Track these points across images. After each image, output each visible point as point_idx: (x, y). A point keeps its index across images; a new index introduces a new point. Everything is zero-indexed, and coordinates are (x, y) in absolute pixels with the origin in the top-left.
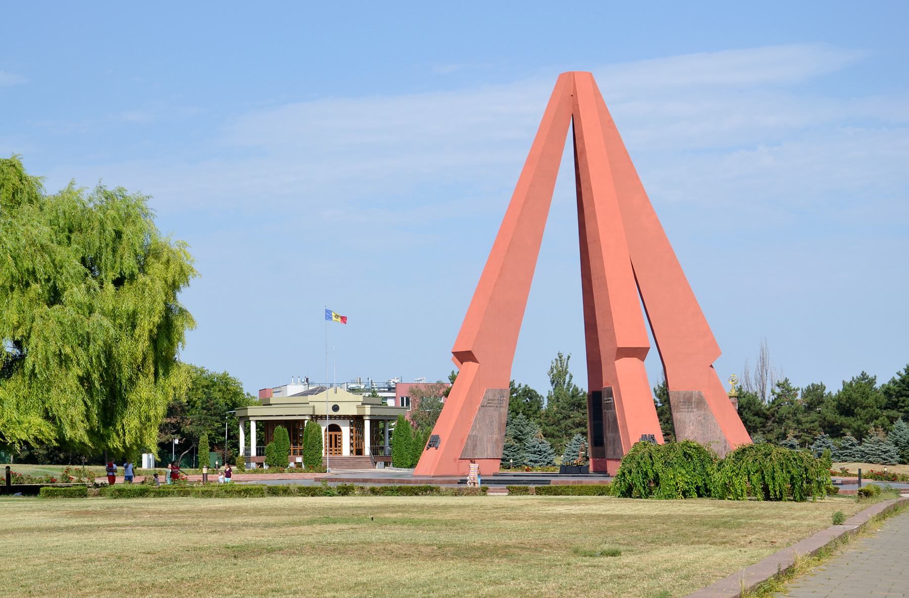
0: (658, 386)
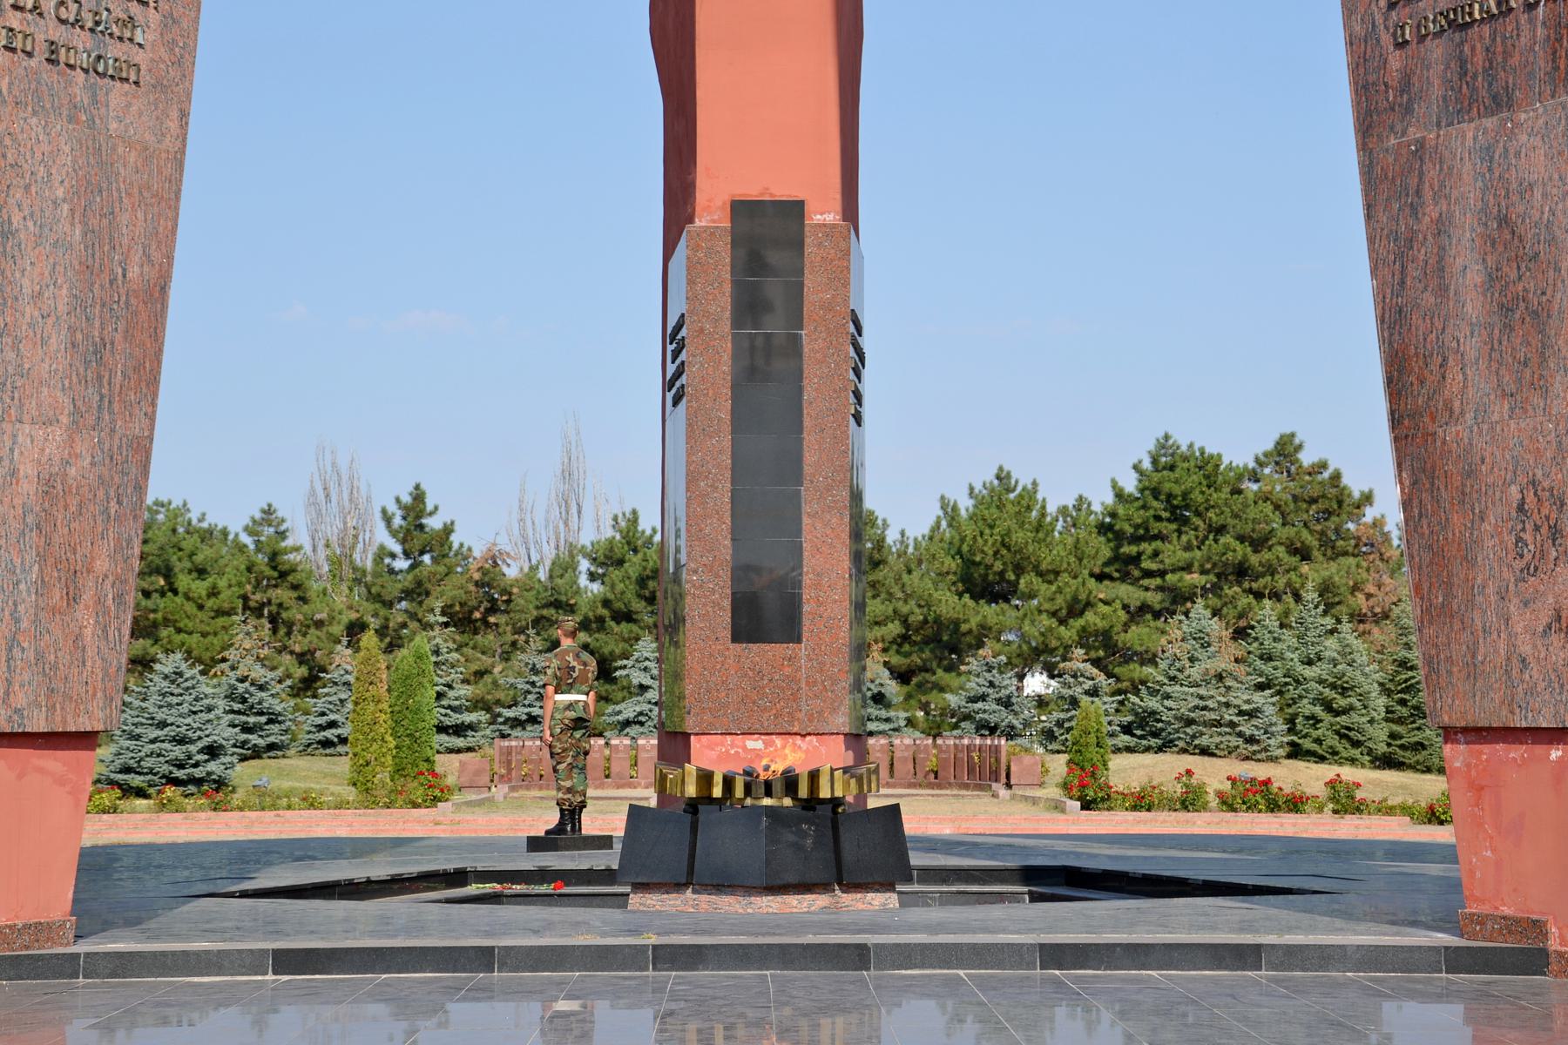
0: (398, 500)
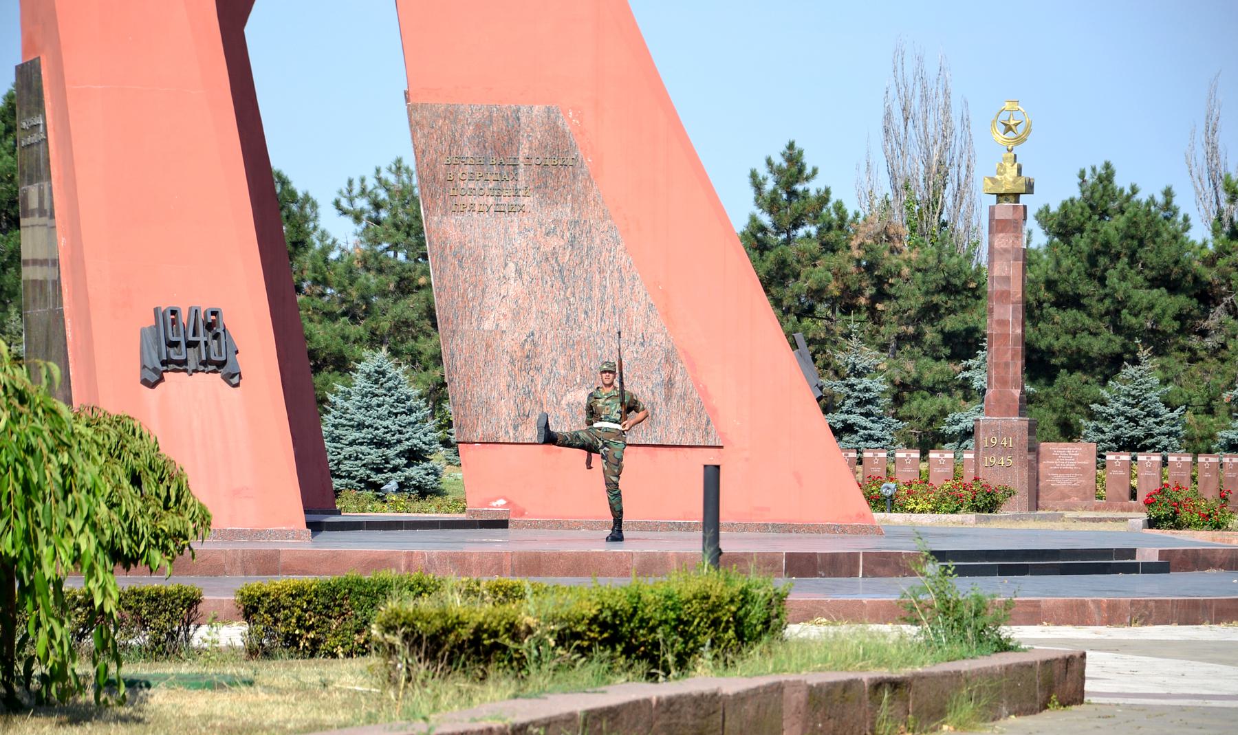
0: (769, 162)
